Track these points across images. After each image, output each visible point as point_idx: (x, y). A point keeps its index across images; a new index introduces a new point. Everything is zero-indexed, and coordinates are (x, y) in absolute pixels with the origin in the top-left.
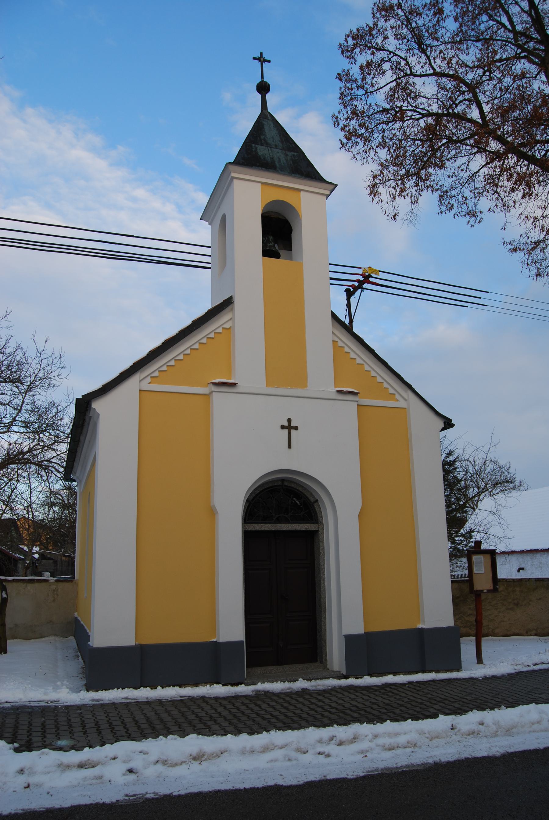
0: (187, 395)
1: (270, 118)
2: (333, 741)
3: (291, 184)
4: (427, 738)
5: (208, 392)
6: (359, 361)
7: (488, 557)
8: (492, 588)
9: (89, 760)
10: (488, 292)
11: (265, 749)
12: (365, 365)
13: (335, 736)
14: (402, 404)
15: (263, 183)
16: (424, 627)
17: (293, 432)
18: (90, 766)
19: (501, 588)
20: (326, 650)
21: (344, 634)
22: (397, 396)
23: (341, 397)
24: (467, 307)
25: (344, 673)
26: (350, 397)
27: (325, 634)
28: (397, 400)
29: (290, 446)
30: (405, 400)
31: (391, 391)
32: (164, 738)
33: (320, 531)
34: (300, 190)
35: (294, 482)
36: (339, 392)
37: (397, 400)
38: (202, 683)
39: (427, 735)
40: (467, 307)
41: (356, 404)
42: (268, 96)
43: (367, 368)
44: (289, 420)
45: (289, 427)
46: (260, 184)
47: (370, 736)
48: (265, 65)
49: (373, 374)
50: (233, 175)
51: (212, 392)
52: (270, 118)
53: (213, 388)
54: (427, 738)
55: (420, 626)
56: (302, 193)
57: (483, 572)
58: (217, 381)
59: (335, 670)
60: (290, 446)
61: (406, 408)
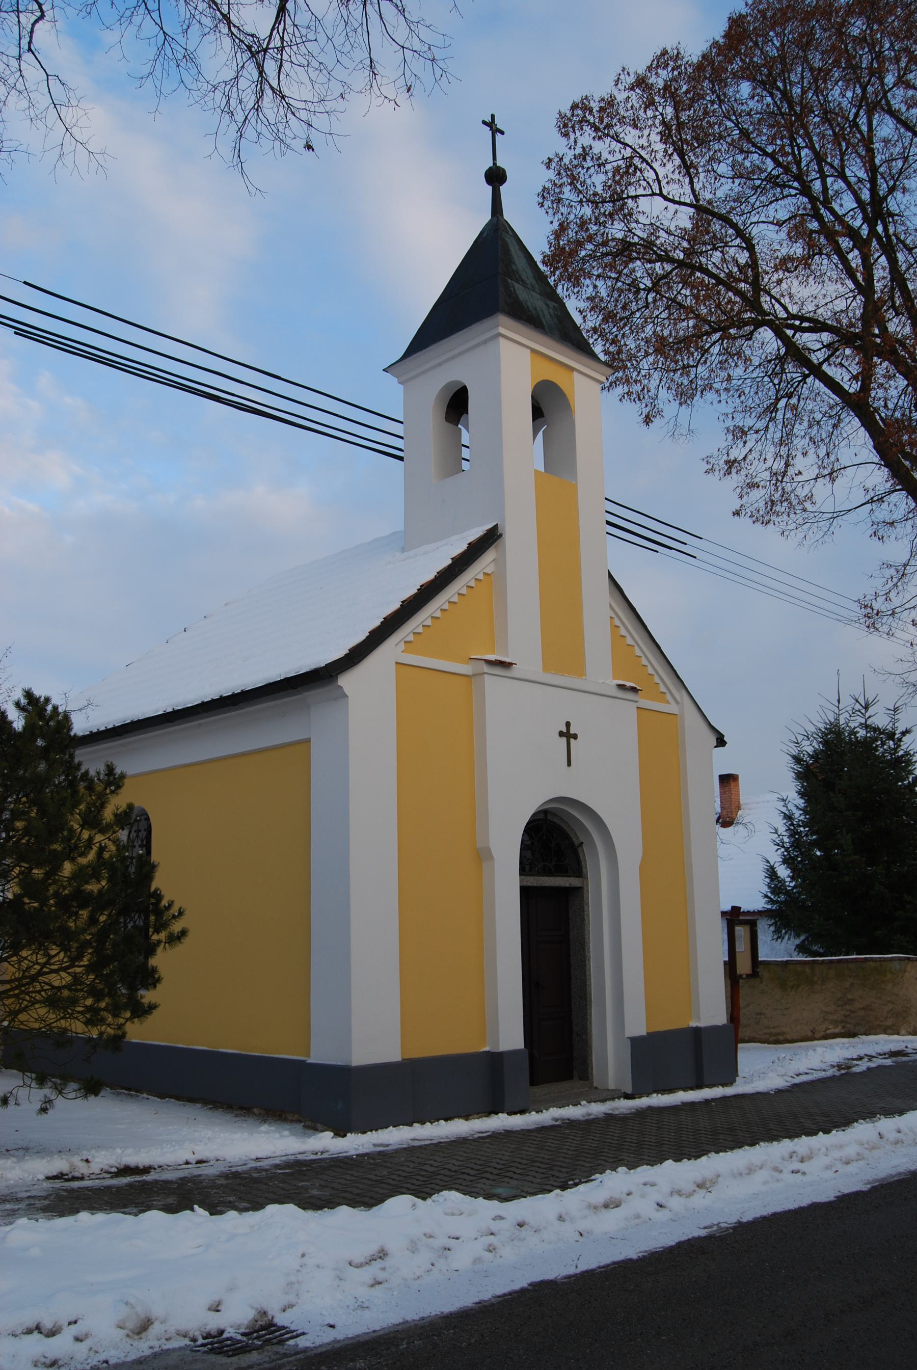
0: (445, 674)
1: (510, 233)
2: (794, 1158)
3: (521, 337)
4: (867, 1149)
5: (470, 673)
6: (629, 641)
7: (747, 928)
8: (750, 972)
9: (611, 1198)
10: (701, 538)
11: (750, 1170)
12: (636, 647)
13: (794, 1152)
14: (673, 708)
15: (533, 351)
16: (699, 1025)
17: (572, 740)
18: (615, 1205)
19: (760, 969)
20: (591, 1061)
21: (631, 1035)
22: (669, 697)
23: (621, 694)
24: (657, 552)
25: (629, 1090)
26: (630, 696)
27: (591, 1037)
28: (668, 702)
29: (569, 764)
30: (677, 702)
31: (663, 689)
32: (614, 1172)
33: (585, 888)
34: (572, 369)
35: (557, 815)
36: (621, 687)
37: (668, 702)
38: (474, 1114)
39: (866, 1146)
40: (657, 552)
41: (635, 705)
42: (503, 189)
43: (638, 652)
44: (568, 724)
45: (568, 735)
46: (529, 351)
47: (824, 1150)
48: (498, 136)
49: (644, 661)
50: (502, 330)
51: (485, 673)
52: (510, 233)
53: (486, 668)
54: (867, 1149)
55: (693, 1024)
56: (575, 374)
57: (743, 950)
58: (492, 657)
59: (610, 1088)
60: (569, 764)
61: (676, 715)
